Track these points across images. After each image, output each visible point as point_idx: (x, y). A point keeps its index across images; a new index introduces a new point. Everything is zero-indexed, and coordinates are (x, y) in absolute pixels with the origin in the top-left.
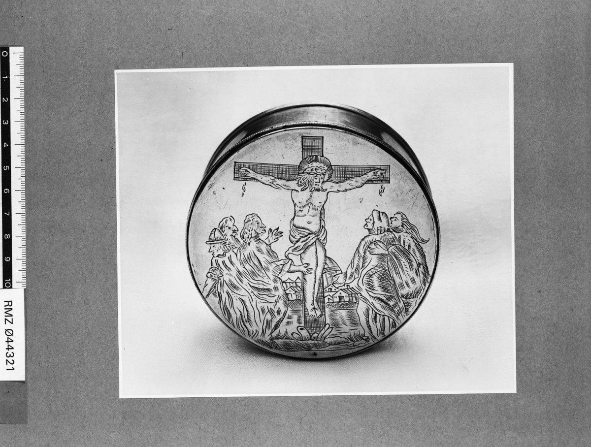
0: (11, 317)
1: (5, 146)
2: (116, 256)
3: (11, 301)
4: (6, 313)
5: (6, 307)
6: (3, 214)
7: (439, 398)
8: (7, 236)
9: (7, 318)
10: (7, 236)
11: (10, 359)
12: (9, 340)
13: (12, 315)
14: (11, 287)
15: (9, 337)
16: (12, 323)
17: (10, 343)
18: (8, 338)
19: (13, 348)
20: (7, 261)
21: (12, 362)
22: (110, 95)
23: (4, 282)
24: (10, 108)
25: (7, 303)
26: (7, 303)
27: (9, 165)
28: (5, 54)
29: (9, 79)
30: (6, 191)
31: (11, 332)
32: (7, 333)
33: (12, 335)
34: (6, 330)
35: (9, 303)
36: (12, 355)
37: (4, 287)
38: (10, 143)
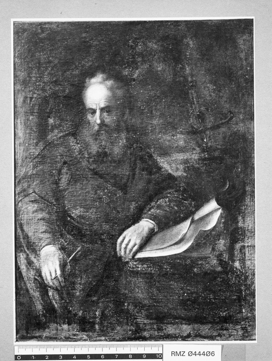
1: (75, 358)
2: (190, 21)
4: (178, 355)
6: (117, 359)
8: (130, 356)
10: (130, 356)
12: (195, 354)
13: (180, 352)
15: (193, 354)
16: (185, 352)
17: (197, 354)
24: (52, 355)
25: (173, 355)
26: (173, 355)
29: (34, 355)
30: (103, 357)
31: (190, 353)
33: (192, 352)
34: (189, 355)
35: (174, 353)
37: (162, 358)
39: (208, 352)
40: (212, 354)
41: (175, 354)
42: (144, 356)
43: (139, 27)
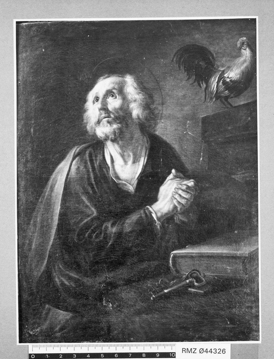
0: (192, 349)
1: (89, 357)
3: (183, 349)
4: (189, 353)
5: (186, 352)
6: (130, 358)
7: (256, 61)
9: (193, 352)
10: (144, 355)
11: (218, 351)
12: (206, 351)
13: (191, 349)
14: (175, 353)
15: (204, 351)
16: (196, 349)
17: (208, 351)
18: (205, 352)
19: (211, 349)
20: (159, 355)
21: (220, 350)
22: (256, 218)
23: (172, 357)
24: (66, 354)
25: (184, 352)
26: (184, 352)
27: (100, 354)
28: (33, 356)
29: (48, 354)
30: (116, 356)
31: (201, 350)
32: (202, 352)
33: (203, 349)
34: (200, 352)
35: (183, 350)
36: (215, 350)
38: (86, 353)
39: (201, 352)
40: (224, 351)
41: (186, 351)
42: (158, 355)
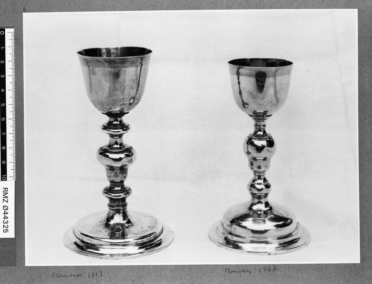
4: (3, 195)
8: (4, 148)
10: (4, 148)
12: (5, 213)
13: (7, 197)
16: (7, 202)
24: (5, 67)
25: (4, 190)
26: (4, 190)
29: (4, 49)
30: (3, 119)
33: (7, 209)
34: (4, 207)
35: (6, 189)
41: (5, 192)
43: (16, 199)
